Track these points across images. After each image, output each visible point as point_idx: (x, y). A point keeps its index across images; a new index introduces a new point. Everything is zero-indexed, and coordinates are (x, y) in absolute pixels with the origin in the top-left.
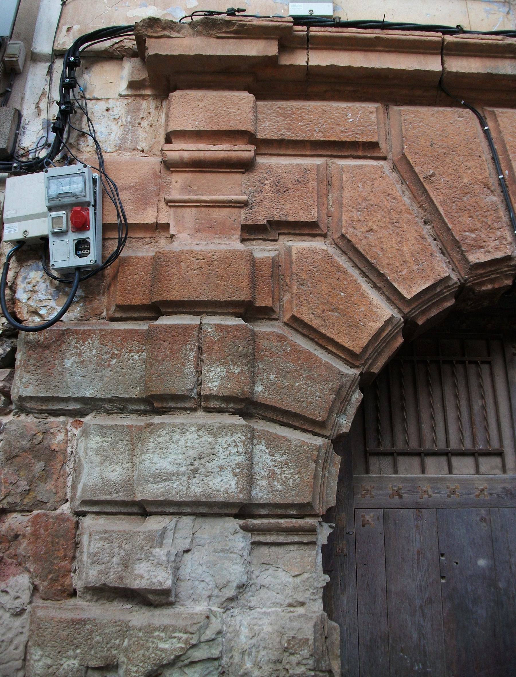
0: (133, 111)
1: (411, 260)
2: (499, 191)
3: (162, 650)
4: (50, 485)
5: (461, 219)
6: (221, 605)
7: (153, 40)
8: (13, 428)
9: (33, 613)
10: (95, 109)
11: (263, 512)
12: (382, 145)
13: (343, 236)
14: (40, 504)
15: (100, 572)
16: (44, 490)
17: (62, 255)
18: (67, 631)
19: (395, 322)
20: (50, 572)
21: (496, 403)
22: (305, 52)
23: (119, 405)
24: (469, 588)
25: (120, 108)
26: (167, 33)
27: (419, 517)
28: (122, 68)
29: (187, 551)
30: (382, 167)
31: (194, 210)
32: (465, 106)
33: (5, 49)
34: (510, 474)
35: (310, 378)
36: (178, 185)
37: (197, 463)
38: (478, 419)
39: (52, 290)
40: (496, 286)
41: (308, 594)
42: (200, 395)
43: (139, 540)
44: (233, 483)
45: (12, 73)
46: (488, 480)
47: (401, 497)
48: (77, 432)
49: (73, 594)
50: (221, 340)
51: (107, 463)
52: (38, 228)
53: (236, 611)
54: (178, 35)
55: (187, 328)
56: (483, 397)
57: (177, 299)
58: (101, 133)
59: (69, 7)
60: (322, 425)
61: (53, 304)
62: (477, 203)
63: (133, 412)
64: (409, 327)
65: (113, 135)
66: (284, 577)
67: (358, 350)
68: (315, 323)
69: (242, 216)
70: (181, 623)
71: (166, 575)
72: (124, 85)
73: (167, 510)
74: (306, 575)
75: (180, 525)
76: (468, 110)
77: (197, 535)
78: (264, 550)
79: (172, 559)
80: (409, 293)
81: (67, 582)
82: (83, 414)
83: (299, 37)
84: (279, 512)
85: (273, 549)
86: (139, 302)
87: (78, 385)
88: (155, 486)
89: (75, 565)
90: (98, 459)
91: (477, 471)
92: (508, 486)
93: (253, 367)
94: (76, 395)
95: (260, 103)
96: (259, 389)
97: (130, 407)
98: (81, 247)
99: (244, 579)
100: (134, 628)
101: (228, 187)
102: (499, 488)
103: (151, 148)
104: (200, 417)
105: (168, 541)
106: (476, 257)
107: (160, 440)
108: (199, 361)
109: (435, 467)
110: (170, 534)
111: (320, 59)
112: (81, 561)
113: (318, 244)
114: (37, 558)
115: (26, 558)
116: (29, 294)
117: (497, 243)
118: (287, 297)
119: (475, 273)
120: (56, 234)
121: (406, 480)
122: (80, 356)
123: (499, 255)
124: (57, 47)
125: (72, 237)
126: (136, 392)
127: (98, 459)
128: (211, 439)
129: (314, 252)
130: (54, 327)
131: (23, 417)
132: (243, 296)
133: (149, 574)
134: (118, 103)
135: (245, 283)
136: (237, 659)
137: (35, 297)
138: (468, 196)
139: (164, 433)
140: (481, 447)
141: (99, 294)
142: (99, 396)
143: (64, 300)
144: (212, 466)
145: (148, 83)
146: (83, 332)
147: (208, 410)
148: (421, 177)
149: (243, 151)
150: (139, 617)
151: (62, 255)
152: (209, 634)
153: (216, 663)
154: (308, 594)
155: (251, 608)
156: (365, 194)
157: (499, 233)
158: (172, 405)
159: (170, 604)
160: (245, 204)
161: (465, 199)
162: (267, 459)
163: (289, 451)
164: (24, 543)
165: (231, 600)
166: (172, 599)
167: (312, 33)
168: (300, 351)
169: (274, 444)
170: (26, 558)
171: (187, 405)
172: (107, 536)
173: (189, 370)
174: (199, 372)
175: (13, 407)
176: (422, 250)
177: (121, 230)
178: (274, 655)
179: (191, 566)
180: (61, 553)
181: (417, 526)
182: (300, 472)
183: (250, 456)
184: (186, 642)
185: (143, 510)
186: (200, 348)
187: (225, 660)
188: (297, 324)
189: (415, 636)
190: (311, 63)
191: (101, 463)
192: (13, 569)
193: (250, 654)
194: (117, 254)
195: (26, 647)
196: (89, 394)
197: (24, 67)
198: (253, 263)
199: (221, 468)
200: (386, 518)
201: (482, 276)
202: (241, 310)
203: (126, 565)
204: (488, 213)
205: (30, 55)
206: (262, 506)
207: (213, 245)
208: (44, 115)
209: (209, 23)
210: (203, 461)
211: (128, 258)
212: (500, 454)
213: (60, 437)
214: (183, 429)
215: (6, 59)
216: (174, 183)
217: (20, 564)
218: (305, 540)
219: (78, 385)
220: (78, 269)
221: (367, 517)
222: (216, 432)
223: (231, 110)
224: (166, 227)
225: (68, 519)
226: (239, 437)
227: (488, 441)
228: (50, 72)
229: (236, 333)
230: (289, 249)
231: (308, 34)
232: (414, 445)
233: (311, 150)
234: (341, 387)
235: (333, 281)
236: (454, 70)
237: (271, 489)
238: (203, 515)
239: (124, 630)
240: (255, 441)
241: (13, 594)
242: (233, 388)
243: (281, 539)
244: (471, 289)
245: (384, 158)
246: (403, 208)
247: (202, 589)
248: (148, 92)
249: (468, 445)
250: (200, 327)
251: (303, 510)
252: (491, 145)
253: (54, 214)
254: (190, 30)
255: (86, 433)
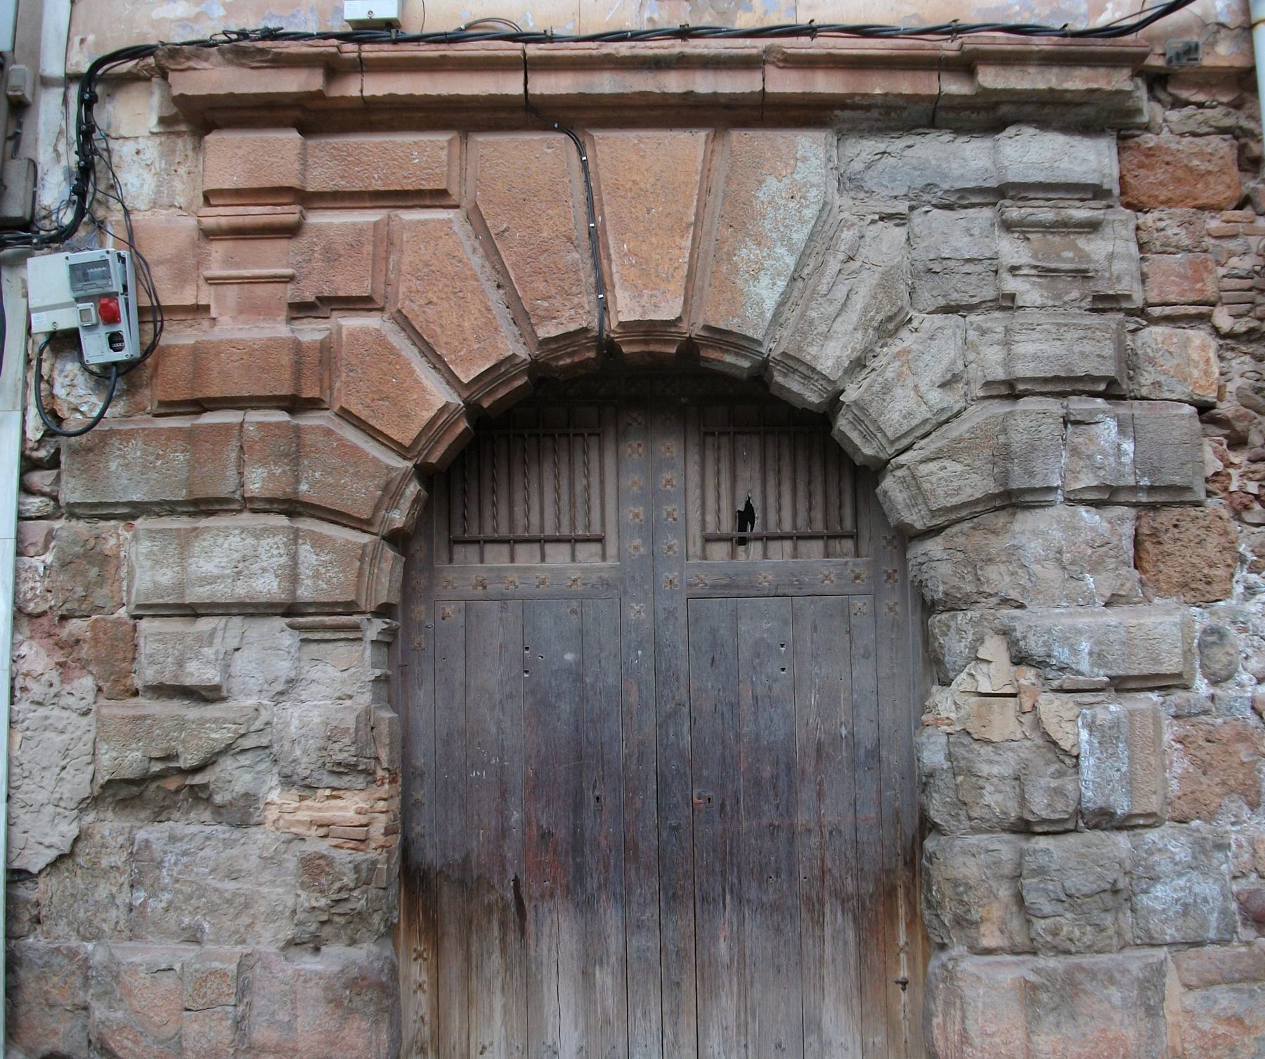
0: (167, 153)
1: (472, 338)
2: (586, 243)
3: (213, 739)
4: (106, 590)
5: (535, 285)
6: (272, 699)
7: (177, 74)
8: (64, 534)
9: (98, 712)
10: (122, 151)
11: (311, 610)
12: (454, 190)
13: (399, 311)
14: (98, 609)
15: (157, 672)
16: (100, 595)
17: (96, 349)
18: (130, 726)
19: (452, 408)
20: (112, 674)
21: (602, 482)
22: (359, 76)
23: (169, 508)
24: (554, 683)
25: (152, 150)
26: (192, 64)
27: (504, 609)
28: (151, 93)
29: (237, 649)
30: (450, 221)
31: (235, 287)
32: (560, 130)
33: (7, 82)
34: (610, 562)
35: (356, 474)
36: (218, 258)
37: (241, 565)
38: (579, 501)
39: (92, 384)
40: (576, 359)
41: (355, 687)
42: (243, 497)
43: (189, 641)
44: (275, 584)
45: (19, 108)
46: (583, 570)
47: (485, 588)
48: (129, 535)
49: (136, 693)
50: (262, 440)
51: (158, 567)
52: (67, 320)
53: (288, 705)
54: (205, 65)
55: (227, 428)
56: (587, 476)
57: (218, 395)
58: (133, 185)
59: (80, 6)
60: (369, 522)
61: (94, 399)
62: (555, 263)
63: (183, 513)
64: (472, 410)
65: (146, 187)
66: (332, 672)
67: (407, 443)
68: (364, 414)
69: (289, 293)
70: (231, 715)
71: (214, 672)
72: (154, 120)
73: (216, 611)
74: (353, 670)
75: (230, 625)
76: (564, 136)
77: (247, 634)
78: (314, 647)
79: (221, 657)
80: (467, 376)
81: (129, 682)
82: (135, 518)
83: (349, 60)
84: (327, 610)
85: (322, 645)
86: (182, 397)
87: (125, 489)
88: (202, 589)
89: (135, 666)
90: (149, 563)
91: (573, 559)
92: (605, 576)
93: (298, 465)
94: (124, 500)
95: (311, 143)
96: (304, 487)
97: (180, 509)
98: (115, 341)
99: (293, 674)
100: (188, 721)
101: (272, 258)
102: (594, 578)
103: (190, 204)
104: (246, 519)
105: (217, 640)
106: (548, 330)
107: (205, 544)
108: (240, 464)
109: (526, 555)
110: (219, 634)
111: (376, 86)
112: (139, 662)
113: (370, 322)
114: (98, 660)
115: (88, 662)
116: (68, 389)
117: (572, 312)
118: (338, 385)
119: (546, 348)
120: (86, 328)
121: (491, 569)
122: (125, 458)
123: (572, 327)
124: (72, 69)
125: (103, 331)
126: (182, 495)
127: (149, 563)
128: (254, 542)
129: (365, 331)
130: (97, 428)
131: (74, 522)
132: (285, 391)
133: (200, 673)
134: (150, 143)
135: (287, 375)
136: (287, 747)
137: (74, 392)
138: (546, 255)
139: (207, 537)
140: (580, 532)
141: (141, 386)
142: (146, 499)
143: (104, 397)
144: (255, 568)
145: (181, 117)
146: (126, 432)
147: (255, 511)
148: (493, 232)
149: (287, 214)
150: (193, 712)
151: (96, 349)
152: (258, 725)
153: (267, 751)
154: (355, 687)
155: (302, 702)
156: (427, 257)
157: (576, 300)
158: (217, 507)
159: (223, 699)
160: (291, 279)
161: (542, 258)
162: (313, 559)
163: (334, 550)
164: (86, 647)
165: (281, 693)
166: (224, 694)
167: (363, 55)
168: (345, 446)
169: (319, 543)
170: (88, 662)
171: (232, 507)
172: (161, 638)
173: (231, 473)
174: (241, 474)
175: (63, 511)
176: (486, 324)
177: (154, 315)
178: (321, 743)
179: (241, 663)
180: (120, 656)
181: (501, 619)
182: (344, 571)
183: (294, 557)
184: (235, 732)
185: (193, 612)
186: (242, 447)
187: (275, 749)
188: (346, 415)
189: (494, 730)
190: (366, 94)
191: (152, 568)
192: (77, 673)
193: (299, 743)
194: (154, 345)
195: (94, 743)
196: (136, 498)
197: (34, 94)
198: (298, 349)
199: (264, 570)
200: (467, 610)
201: (555, 350)
202: (286, 404)
203: (180, 664)
204: (566, 276)
205: (38, 81)
206: (310, 604)
207: (256, 330)
208: (64, 162)
209: (241, 48)
210: (247, 563)
211: (169, 346)
212: (600, 540)
213: (112, 541)
214: (226, 532)
215: (10, 93)
216: (214, 254)
217: (83, 668)
218: (351, 636)
219: (125, 489)
220: (115, 364)
221: (448, 610)
222: (258, 534)
223: (273, 160)
224: (207, 308)
225: (126, 623)
226: (280, 539)
227: (588, 526)
228: (65, 101)
229: (277, 431)
230: (340, 327)
231: (359, 56)
232: (504, 531)
233: (371, 200)
234: (388, 484)
235: (384, 366)
236: (538, 92)
237: (317, 589)
238: (252, 615)
239: (181, 724)
240: (300, 541)
241: (78, 695)
242: (278, 490)
243: (328, 636)
244: (546, 365)
245: (457, 207)
246: (469, 273)
247: (253, 685)
248: (183, 128)
249: (565, 531)
250: (242, 425)
251: (350, 608)
252: (587, 181)
253: (82, 306)
254: (220, 58)
255: (135, 538)
